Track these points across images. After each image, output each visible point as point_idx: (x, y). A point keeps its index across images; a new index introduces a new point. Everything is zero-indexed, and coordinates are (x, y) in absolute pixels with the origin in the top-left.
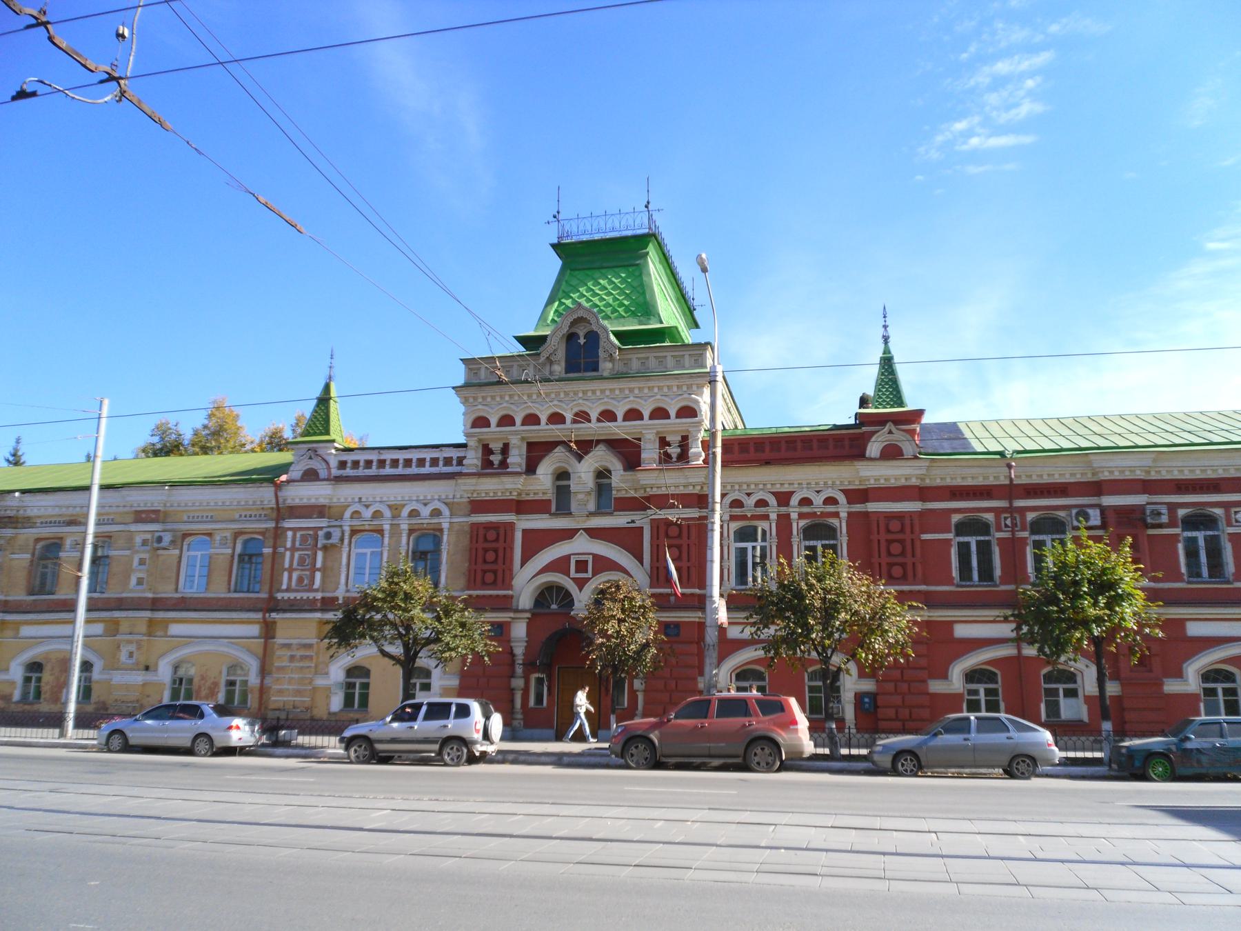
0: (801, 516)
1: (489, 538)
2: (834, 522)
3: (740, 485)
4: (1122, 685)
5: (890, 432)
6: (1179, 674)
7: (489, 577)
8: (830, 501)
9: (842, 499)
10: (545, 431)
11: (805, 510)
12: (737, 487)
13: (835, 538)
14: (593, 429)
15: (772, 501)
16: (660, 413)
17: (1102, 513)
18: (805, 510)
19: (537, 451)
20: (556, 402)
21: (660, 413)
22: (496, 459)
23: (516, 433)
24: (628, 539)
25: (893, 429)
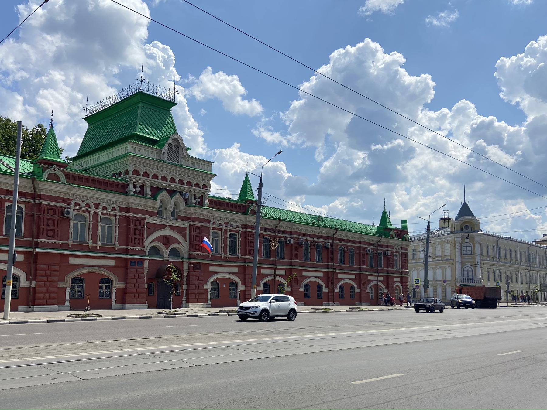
0: (103, 214)
5: (54, 170)
9: (118, 209)
10: (159, 183)
14: (176, 186)
16: (155, 176)
18: (105, 211)
21: (197, 185)
25: (56, 169)
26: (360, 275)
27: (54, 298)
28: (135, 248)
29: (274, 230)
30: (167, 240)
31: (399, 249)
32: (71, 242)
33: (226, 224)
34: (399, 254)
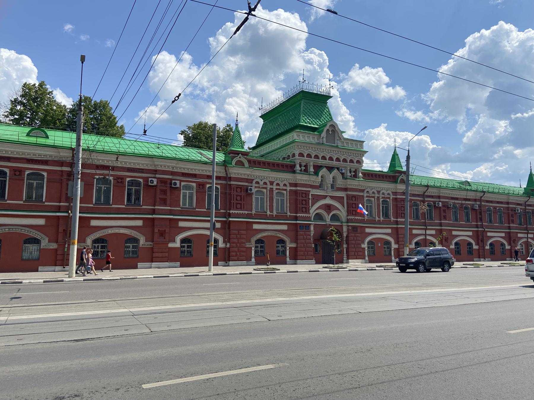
0: (277, 189)
1: (303, 196)
4: (58, 245)
6: (174, 241)
7: (304, 210)
8: (389, 194)
10: (320, 162)
11: (257, 185)
14: (334, 163)
15: (268, 183)
21: (316, 157)
24: (339, 199)
32: (254, 212)
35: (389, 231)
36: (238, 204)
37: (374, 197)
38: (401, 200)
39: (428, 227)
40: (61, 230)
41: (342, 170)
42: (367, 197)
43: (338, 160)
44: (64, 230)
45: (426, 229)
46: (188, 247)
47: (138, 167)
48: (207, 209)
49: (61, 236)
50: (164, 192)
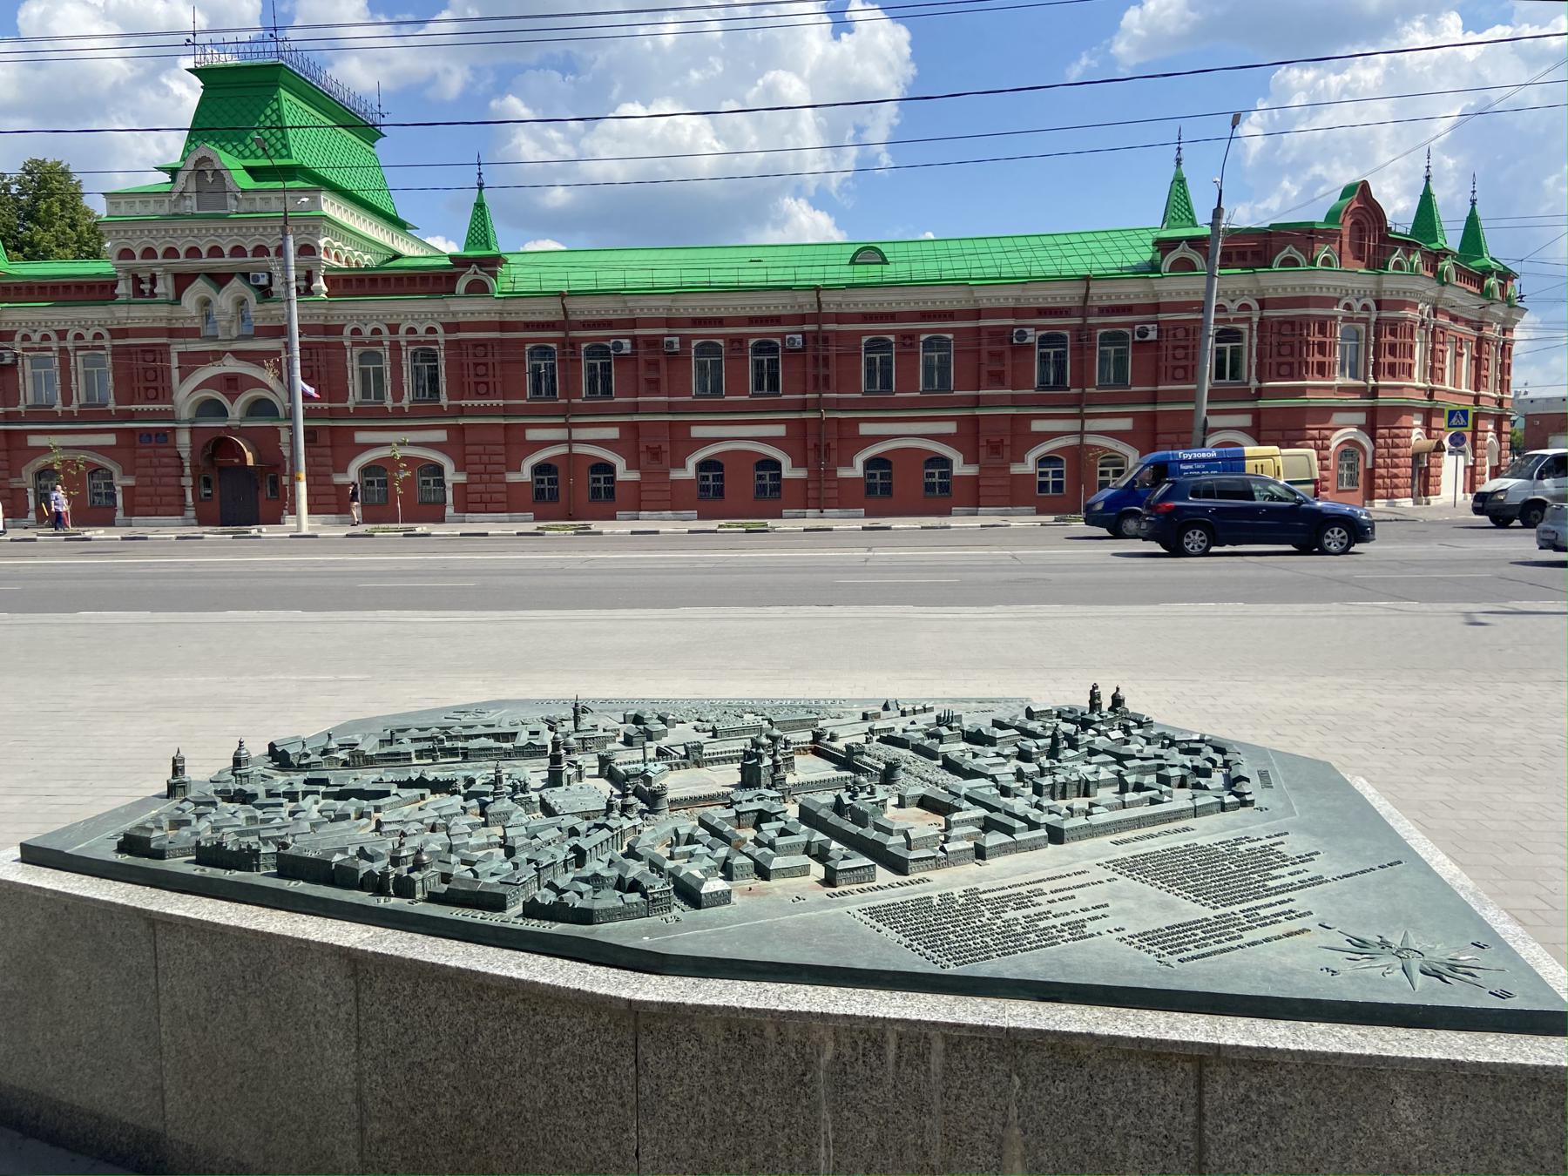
2: (379, 349)
3: (358, 315)
4: (980, 468)
8: (431, 330)
10: (184, 264)
12: (43, 324)
13: (436, 361)
14: (226, 262)
17: (1159, 331)
19: (183, 281)
20: (168, 239)
21: (171, 252)
22: (146, 287)
23: (159, 265)
26: (1153, 416)
27: (170, 505)
28: (476, 403)
29: (1084, 311)
30: (232, 384)
31: (1366, 308)
32: (350, 404)
33: (394, 329)
34: (1251, 329)
35: (441, 436)
36: (1285, 366)
37: (1366, 321)
38: (476, 346)
39: (1087, 411)
40: (810, 445)
41: (256, 278)
42: (1345, 319)
43: (238, 251)
44: (815, 445)
45: (1082, 417)
46: (942, 475)
47: (907, 308)
48: (863, 394)
49: (811, 455)
50: (997, 356)
